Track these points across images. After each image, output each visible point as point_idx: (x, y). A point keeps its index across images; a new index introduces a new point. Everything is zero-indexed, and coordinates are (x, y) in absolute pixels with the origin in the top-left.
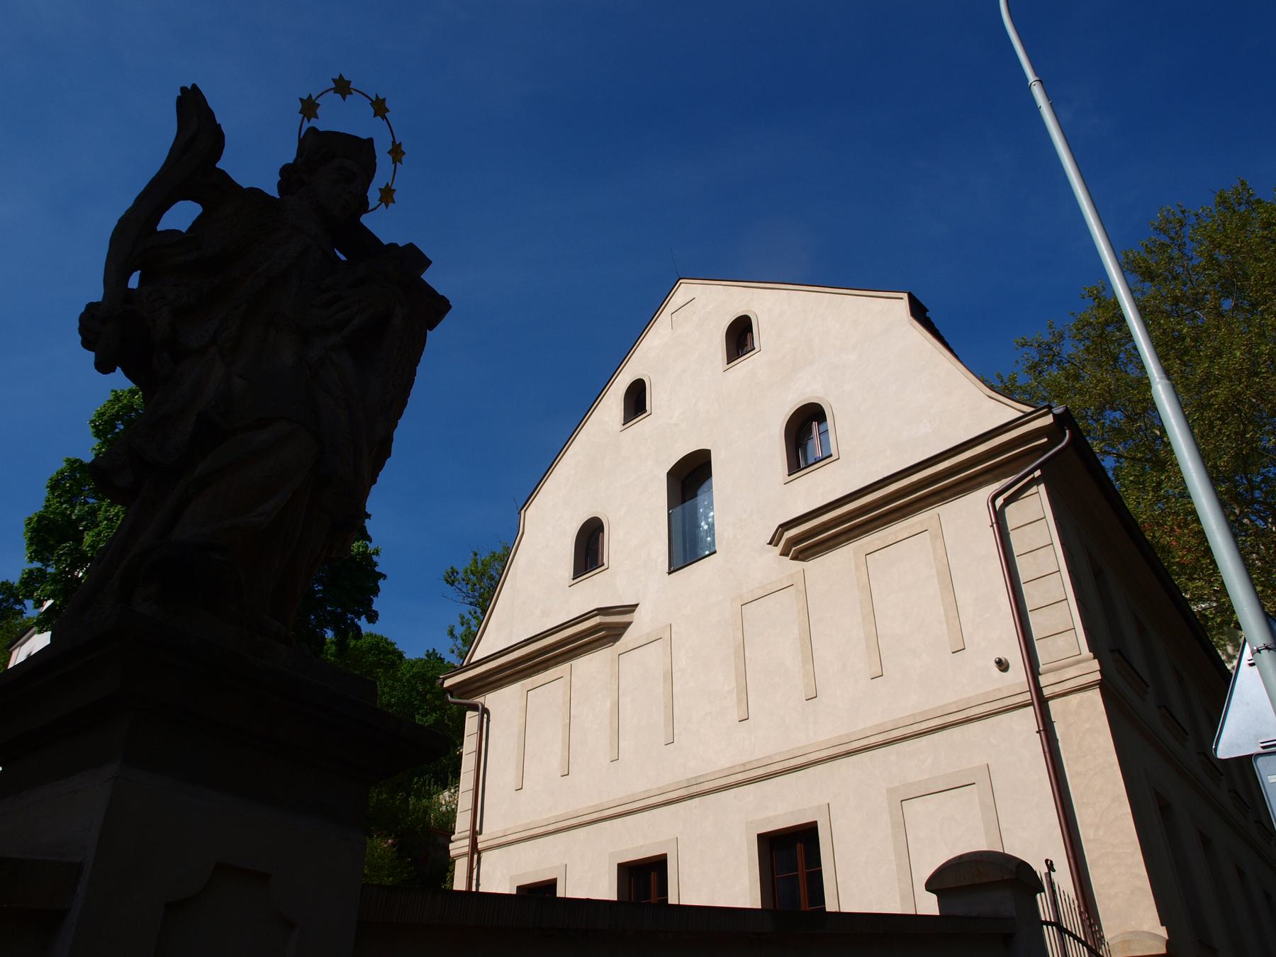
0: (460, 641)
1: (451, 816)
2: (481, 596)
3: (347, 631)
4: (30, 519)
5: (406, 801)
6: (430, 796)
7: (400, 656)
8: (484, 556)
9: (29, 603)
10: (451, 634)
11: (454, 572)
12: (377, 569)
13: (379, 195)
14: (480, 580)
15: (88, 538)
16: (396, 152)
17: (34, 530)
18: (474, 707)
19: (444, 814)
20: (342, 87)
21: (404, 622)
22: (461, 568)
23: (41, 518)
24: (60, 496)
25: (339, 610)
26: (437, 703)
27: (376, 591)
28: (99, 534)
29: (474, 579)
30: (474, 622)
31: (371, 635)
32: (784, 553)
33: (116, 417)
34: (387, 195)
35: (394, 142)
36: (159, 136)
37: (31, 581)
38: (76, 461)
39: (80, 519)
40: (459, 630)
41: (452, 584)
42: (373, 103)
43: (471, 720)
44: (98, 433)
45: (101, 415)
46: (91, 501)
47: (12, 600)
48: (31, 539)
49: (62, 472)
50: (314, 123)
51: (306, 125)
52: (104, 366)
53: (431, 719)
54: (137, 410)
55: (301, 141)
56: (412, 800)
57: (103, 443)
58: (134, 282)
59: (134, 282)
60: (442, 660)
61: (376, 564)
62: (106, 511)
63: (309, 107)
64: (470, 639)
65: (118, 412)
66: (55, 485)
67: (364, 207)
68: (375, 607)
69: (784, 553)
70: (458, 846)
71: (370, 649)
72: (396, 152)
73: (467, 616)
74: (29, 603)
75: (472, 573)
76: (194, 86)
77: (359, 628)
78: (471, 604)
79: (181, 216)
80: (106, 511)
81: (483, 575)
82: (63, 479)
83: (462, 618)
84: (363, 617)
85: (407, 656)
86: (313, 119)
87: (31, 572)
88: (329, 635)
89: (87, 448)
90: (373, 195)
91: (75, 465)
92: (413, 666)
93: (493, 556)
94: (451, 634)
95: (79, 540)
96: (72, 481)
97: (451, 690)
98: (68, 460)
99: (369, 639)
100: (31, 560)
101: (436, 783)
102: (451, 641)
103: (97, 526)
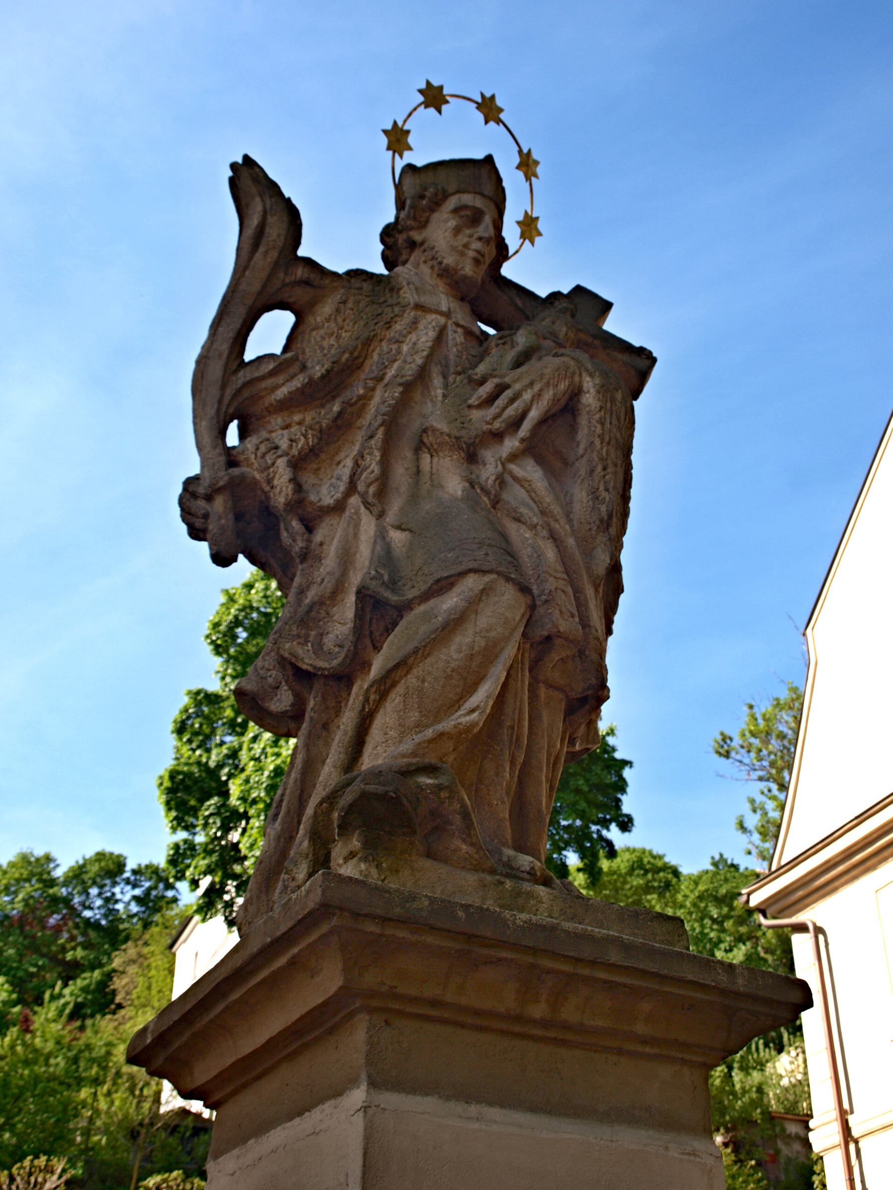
0: (756, 837)
1: (802, 1089)
2: (772, 764)
3: (594, 850)
4: (161, 777)
5: (729, 1076)
6: (761, 1065)
7: (676, 873)
8: (764, 707)
9: (183, 886)
10: (742, 827)
11: (726, 738)
12: (618, 755)
13: (518, 231)
14: (766, 742)
15: (235, 788)
16: (527, 164)
17: (170, 791)
18: (802, 928)
19: (787, 1090)
20: (434, 97)
21: (676, 820)
22: (734, 733)
23: (173, 774)
24: (190, 741)
25: (578, 823)
26: (743, 929)
27: (621, 786)
28: (247, 781)
29: (756, 742)
30: (770, 805)
31: (628, 849)
32: (55, 860)
33: (237, 622)
34: (529, 227)
35: (520, 151)
36: (217, 239)
37: (179, 856)
38: (198, 693)
39: (220, 766)
40: (753, 821)
41: (727, 755)
42: (479, 107)
43: (801, 944)
44: (219, 650)
45: (216, 625)
46: (228, 739)
47: (161, 886)
48: (168, 803)
49: (186, 710)
50: (409, 158)
51: (400, 164)
52: (222, 559)
53: (738, 955)
54: (258, 609)
55: (398, 187)
56: (737, 1076)
57: (227, 661)
58: (232, 437)
59: (232, 437)
60: (735, 867)
61: (614, 750)
62: (250, 749)
63: (397, 139)
64: (772, 831)
65: (236, 617)
66: (181, 729)
67: (502, 253)
68: (626, 809)
69: (55, 860)
70: (823, 1136)
71: (631, 871)
72: (527, 164)
73: (759, 798)
74: (183, 886)
75: (753, 734)
76: (246, 158)
77: (610, 844)
78: (761, 779)
79: (271, 333)
80: (250, 749)
81: (768, 734)
82: (189, 718)
83: (752, 801)
84: (613, 826)
85: (685, 870)
86: (406, 154)
87: (177, 847)
88: (572, 859)
89: (210, 674)
90: (511, 233)
91: (205, 700)
92: (696, 883)
93: (778, 705)
94: (742, 827)
95: (225, 794)
96: (199, 719)
97: (762, 910)
98: (189, 692)
99: (627, 856)
100: (174, 830)
101: (766, 1045)
102: (742, 840)
103: (243, 770)
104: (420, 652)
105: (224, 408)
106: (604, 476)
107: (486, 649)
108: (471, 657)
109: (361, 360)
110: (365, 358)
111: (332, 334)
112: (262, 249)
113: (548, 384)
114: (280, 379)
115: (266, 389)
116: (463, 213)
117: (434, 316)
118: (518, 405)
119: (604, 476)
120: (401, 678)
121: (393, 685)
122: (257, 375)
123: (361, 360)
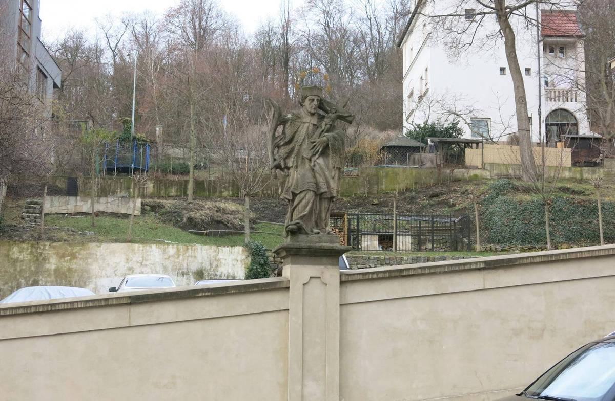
114: (281, 141)
118: (317, 149)
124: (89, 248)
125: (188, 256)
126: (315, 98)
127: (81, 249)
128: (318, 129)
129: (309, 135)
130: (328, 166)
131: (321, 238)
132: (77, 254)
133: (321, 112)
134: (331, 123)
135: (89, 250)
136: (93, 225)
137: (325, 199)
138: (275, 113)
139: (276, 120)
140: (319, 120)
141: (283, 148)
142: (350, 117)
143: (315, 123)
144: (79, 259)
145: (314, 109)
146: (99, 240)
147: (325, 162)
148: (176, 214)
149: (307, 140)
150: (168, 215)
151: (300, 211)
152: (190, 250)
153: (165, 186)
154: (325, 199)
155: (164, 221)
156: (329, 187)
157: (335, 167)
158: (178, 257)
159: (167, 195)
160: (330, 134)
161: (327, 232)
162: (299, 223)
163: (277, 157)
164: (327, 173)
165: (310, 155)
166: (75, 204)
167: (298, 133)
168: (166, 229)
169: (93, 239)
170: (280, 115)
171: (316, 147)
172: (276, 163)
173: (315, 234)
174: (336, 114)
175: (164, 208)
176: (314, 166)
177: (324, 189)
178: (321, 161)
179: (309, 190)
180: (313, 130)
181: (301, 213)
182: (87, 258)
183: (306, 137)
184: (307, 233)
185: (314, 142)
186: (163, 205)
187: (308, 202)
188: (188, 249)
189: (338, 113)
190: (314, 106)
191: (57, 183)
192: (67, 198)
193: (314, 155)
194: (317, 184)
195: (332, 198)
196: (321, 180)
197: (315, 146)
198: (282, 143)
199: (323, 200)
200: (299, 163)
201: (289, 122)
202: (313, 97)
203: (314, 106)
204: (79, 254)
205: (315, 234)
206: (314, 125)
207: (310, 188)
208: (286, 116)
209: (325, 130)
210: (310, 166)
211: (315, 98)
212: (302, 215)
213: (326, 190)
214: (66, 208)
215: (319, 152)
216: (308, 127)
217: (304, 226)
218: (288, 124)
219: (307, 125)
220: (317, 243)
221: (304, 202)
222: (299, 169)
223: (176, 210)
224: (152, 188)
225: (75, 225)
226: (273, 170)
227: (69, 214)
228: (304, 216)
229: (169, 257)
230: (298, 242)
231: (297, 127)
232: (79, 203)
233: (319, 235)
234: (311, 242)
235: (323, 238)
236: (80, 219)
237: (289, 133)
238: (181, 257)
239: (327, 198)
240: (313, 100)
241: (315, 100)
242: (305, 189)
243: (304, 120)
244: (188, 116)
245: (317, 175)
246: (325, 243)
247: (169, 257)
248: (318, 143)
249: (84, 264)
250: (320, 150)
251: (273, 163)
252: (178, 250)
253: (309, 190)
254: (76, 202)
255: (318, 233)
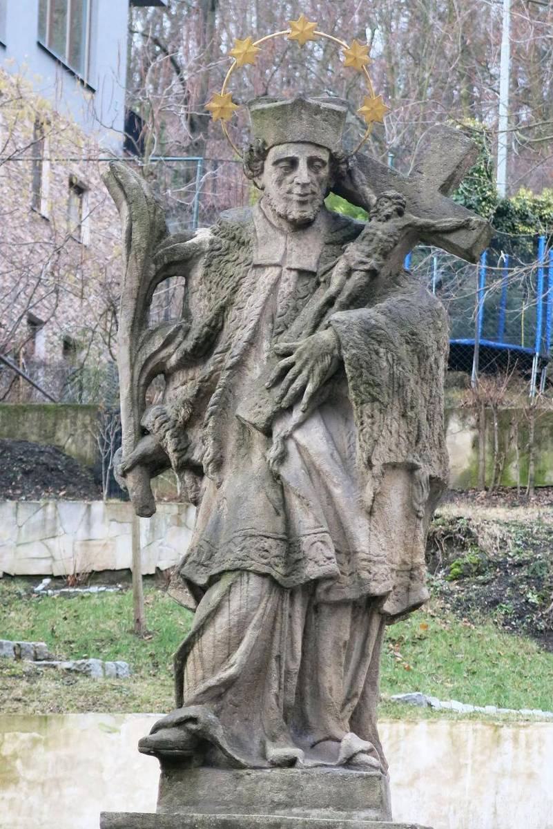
104: (481, 440)
105: (136, 383)
106: (362, 430)
107: (239, 622)
108: (230, 630)
109: (220, 325)
110: (223, 322)
111: (205, 296)
112: (133, 253)
113: (317, 361)
114: (170, 349)
115: (163, 358)
116: (283, 164)
117: (270, 269)
118: (297, 384)
119: (362, 430)
120: (190, 650)
121: (188, 654)
122: (154, 349)
123: (220, 325)
124: (67, 735)
125: (502, 774)
126: (303, 154)
127: (35, 742)
128: (320, 290)
129: (276, 321)
130: (345, 462)
131: (298, 787)
132: (18, 763)
133: (341, 207)
134: (372, 262)
135: (67, 744)
136: (138, 630)
137: (338, 605)
138: (135, 225)
139: (142, 255)
140: (329, 249)
141: (180, 377)
142: (463, 232)
143: (309, 263)
144: (23, 785)
145: (302, 203)
146: (133, 698)
147: (331, 437)
148: (524, 572)
149: (265, 345)
150: (488, 576)
151: (207, 666)
152: (508, 746)
153: (523, 439)
154: (338, 605)
155: (462, 607)
156: (346, 550)
157: (377, 463)
158: (457, 777)
159: (533, 480)
160: (355, 314)
161: (342, 756)
162: (193, 720)
163: (149, 420)
164: (337, 491)
165: (268, 410)
166: (81, 534)
167: (233, 313)
168: (463, 644)
169: (107, 697)
170: (158, 233)
171: (290, 376)
172: (147, 444)
173: (276, 765)
174: (400, 222)
175: (475, 543)
176: (282, 458)
177: (319, 560)
178: (314, 437)
179: (242, 571)
180: (294, 295)
181: (214, 670)
182: (57, 783)
183: (265, 329)
184: (234, 765)
185: (287, 354)
186: (468, 533)
187: (241, 626)
188: (498, 741)
189: (410, 217)
190: (297, 190)
191: (60, 434)
192: (50, 509)
193: (283, 412)
194: (289, 540)
195: (373, 602)
196: (306, 521)
197: (286, 370)
198: (173, 361)
199: (325, 610)
200: (231, 447)
201: (202, 262)
202: (291, 152)
203: (297, 190)
204: (27, 764)
205: (276, 765)
206: (302, 273)
207: (246, 564)
208: (184, 238)
209: (342, 298)
210: (264, 457)
211: (303, 154)
212: (212, 681)
213: (333, 567)
214: (46, 553)
215: (305, 399)
216: (276, 285)
217: (219, 733)
218: (199, 272)
219: (272, 273)
220: (277, 805)
221: (222, 621)
222: (228, 472)
223: (527, 555)
224: (469, 452)
225: (63, 628)
226: (130, 476)
227: (59, 577)
228: (229, 684)
229: (416, 777)
230: (193, 803)
231: (231, 284)
232: (101, 530)
233: (289, 772)
234: (249, 805)
235: (309, 787)
236: (95, 601)
237: (202, 312)
238: (468, 780)
239: (344, 603)
240: (293, 163)
241: (302, 164)
242: (226, 566)
243: (259, 256)
244: (215, 180)
245: (295, 502)
246: (316, 806)
247: (416, 777)
248: (300, 354)
249: (46, 808)
250: (310, 388)
251: (135, 445)
252: (456, 745)
253: (242, 571)
254: (89, 525)
255: (292, 762)
